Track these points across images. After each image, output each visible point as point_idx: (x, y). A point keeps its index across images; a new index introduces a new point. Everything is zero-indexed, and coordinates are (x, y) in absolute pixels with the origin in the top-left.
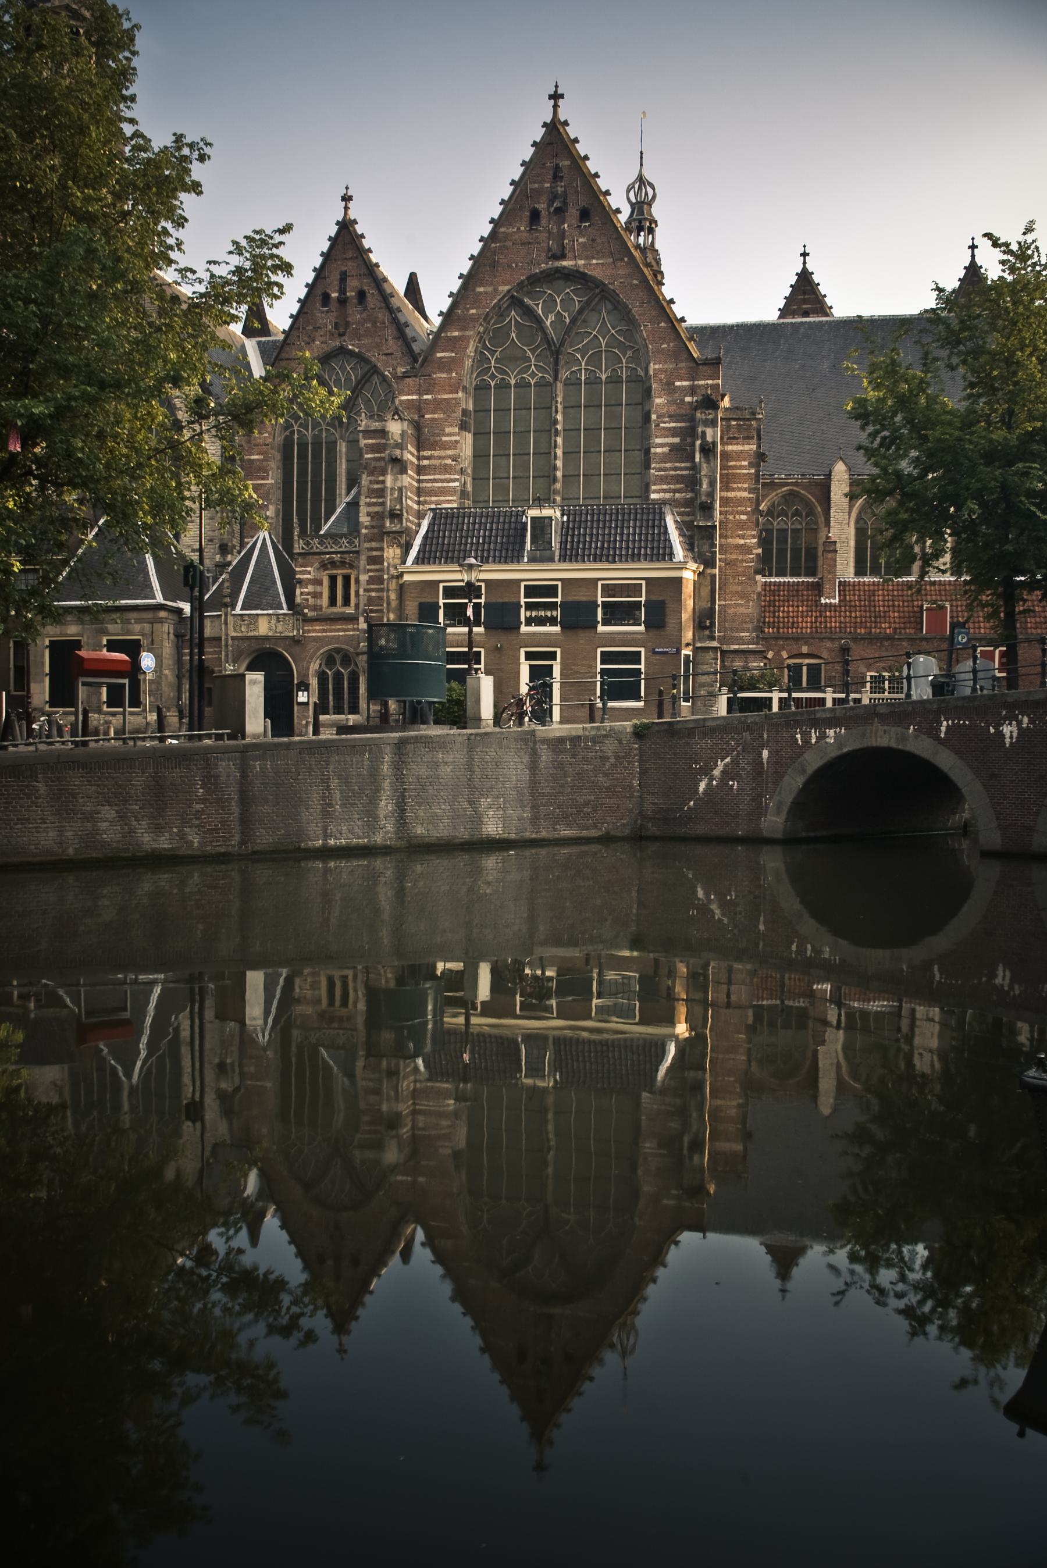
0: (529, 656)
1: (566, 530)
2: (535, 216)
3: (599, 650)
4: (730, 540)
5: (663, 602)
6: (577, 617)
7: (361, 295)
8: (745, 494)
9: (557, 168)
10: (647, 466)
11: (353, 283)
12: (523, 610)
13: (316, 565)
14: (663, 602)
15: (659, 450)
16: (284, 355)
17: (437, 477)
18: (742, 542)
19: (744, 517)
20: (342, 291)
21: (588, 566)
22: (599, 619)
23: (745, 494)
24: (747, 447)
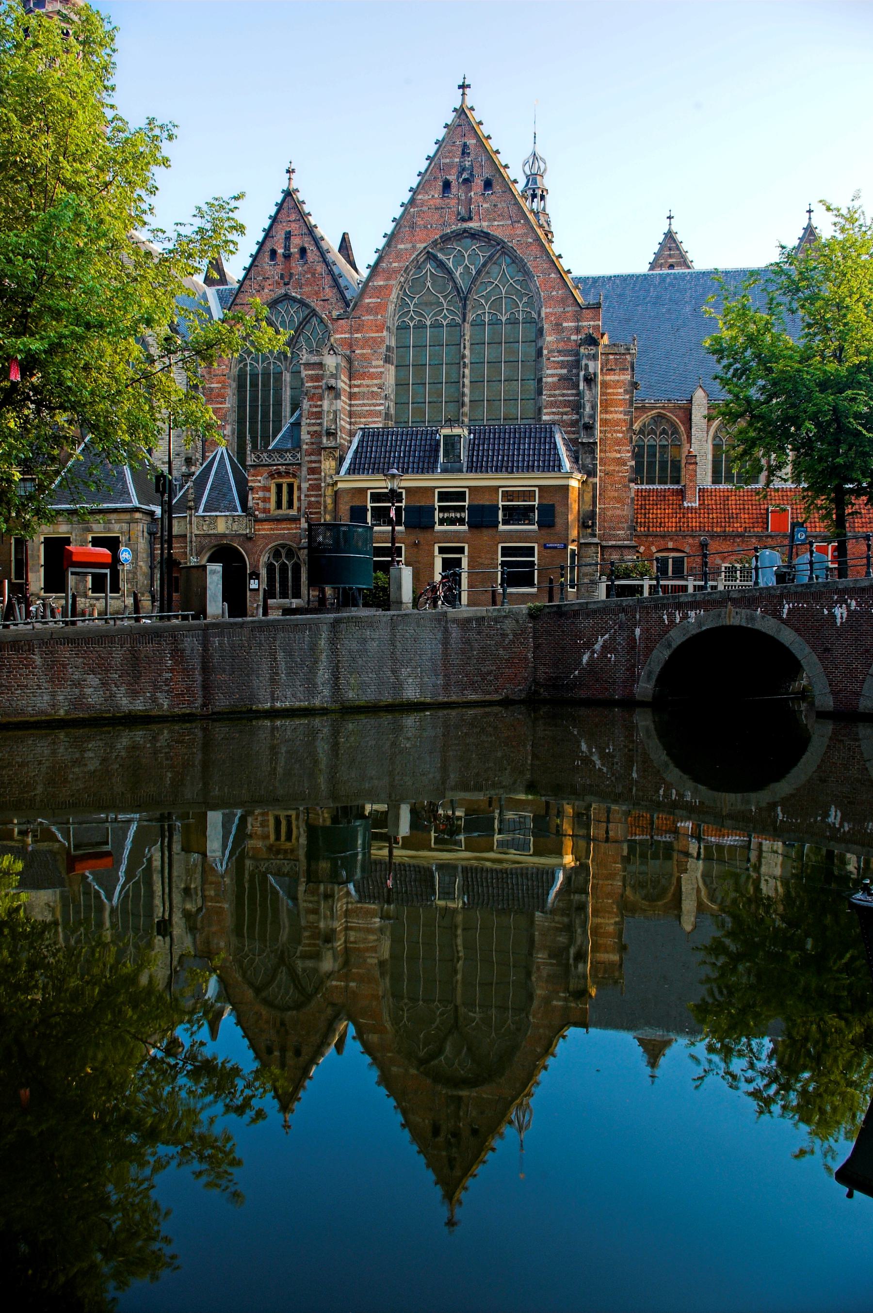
0: (442, 550)
1: (472, 446)
2: (447, 185)
3: (500, 545)
4: (608, 454)
5: (553, 506)
6: (482, 518)
7: (303, 251)
8: (621, 416)
9: (465, 145)
10: (540, 393)
11: (296, 242)
12: (437, 512)
13: (266, 475)
14: (553, 506)
15: (549, 380)
16: (238, 301)
17: (366, 402)
18: (618, 456)
19: (620, 435)
20: (287, 248)
21: (500, 475)
22: (500, 520)
23: (621, 416)
24: (622, 377)
